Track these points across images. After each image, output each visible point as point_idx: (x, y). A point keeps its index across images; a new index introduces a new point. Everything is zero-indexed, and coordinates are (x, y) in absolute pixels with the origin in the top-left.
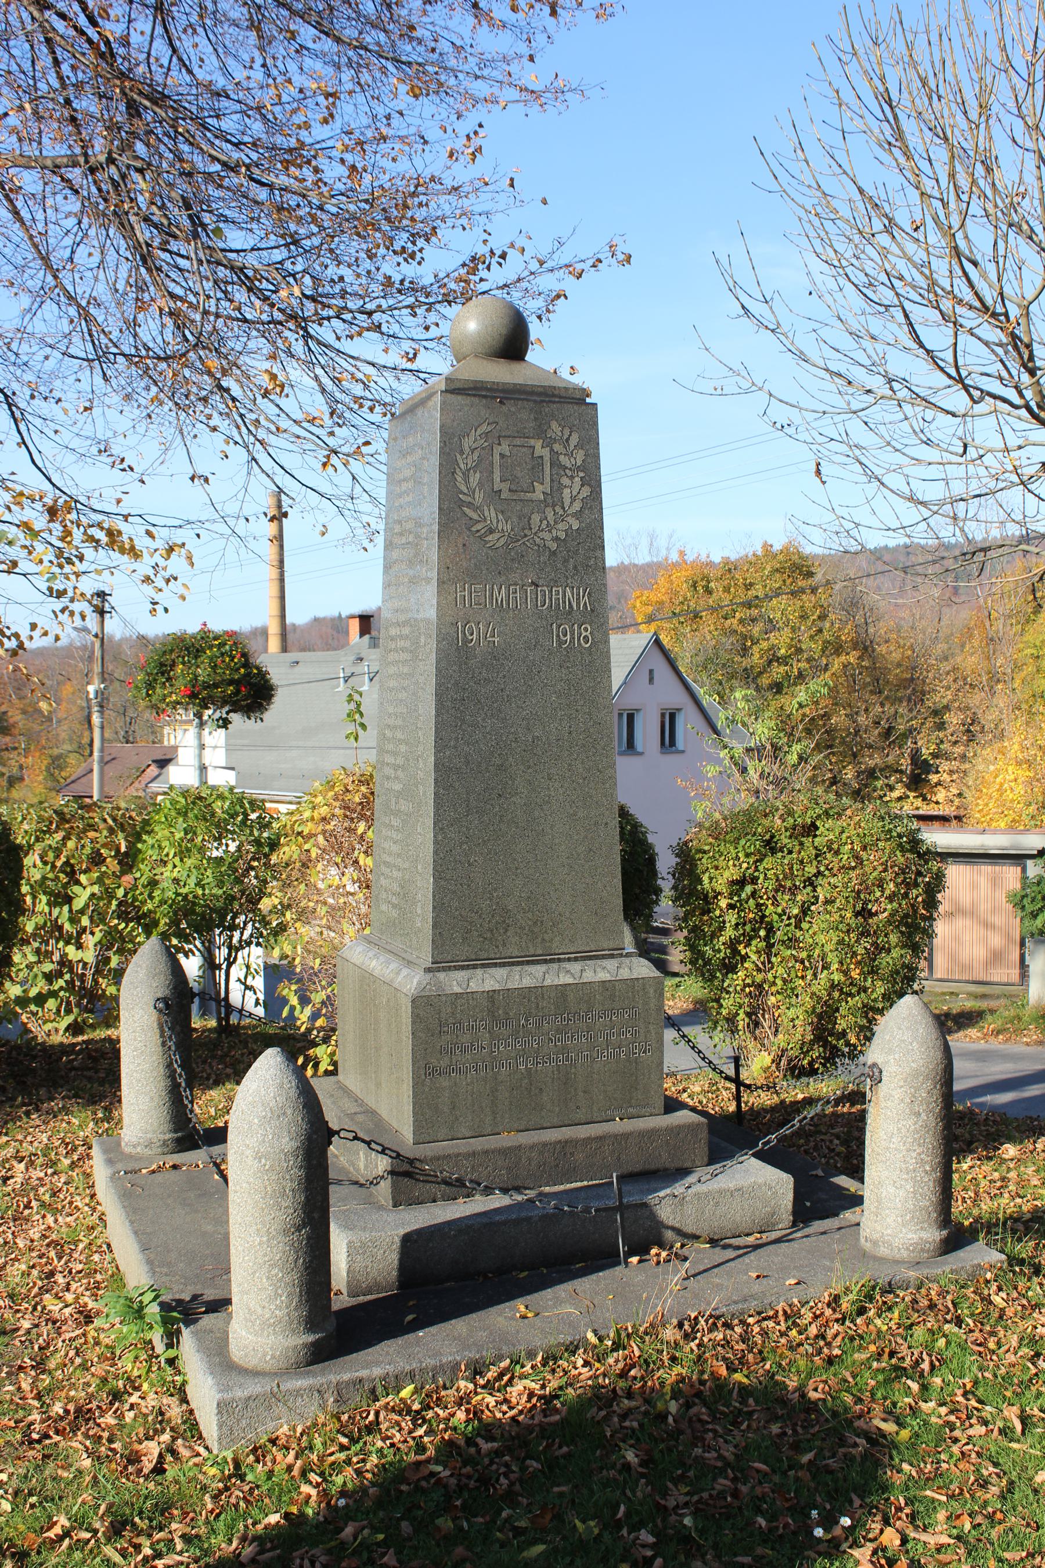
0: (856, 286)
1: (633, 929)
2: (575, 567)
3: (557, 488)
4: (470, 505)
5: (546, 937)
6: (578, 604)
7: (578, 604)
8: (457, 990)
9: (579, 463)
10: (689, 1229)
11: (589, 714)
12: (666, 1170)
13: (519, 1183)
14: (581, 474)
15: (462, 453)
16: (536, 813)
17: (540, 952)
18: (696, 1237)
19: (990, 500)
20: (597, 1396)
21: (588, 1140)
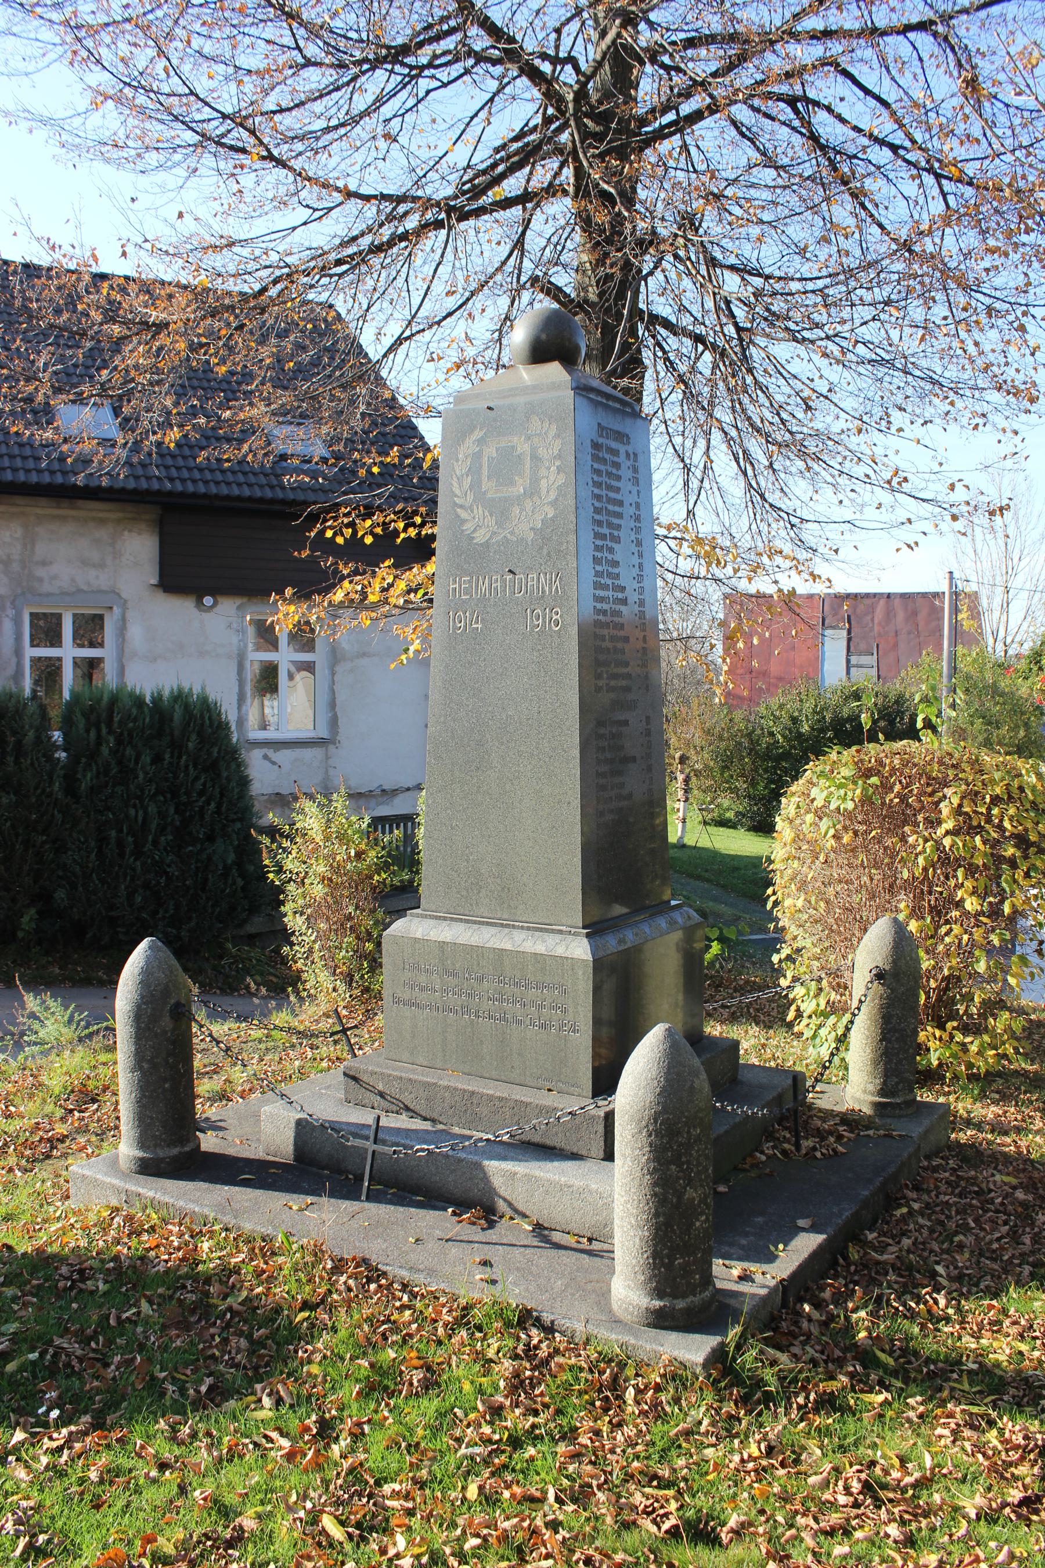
0: (967, 160)
1: (988, 962)
2: (549, 554)
3: (535, 480)
4: (461, 507)
5: (512, 904)
6: (550, 589)
7: (550, 589)
8: (418, 935)
9: (556, 452)
10: (521, 1207)
11: (557, 695)
12: (561, 1150)
13: (435, 1116)
14: (558, 463)
15: (457, 460)
16: (508, 787)
17: (506, 916)
18: (524, 1216)
19: (391, 322)
20: (172, 1279)
21: (491, 1098)
